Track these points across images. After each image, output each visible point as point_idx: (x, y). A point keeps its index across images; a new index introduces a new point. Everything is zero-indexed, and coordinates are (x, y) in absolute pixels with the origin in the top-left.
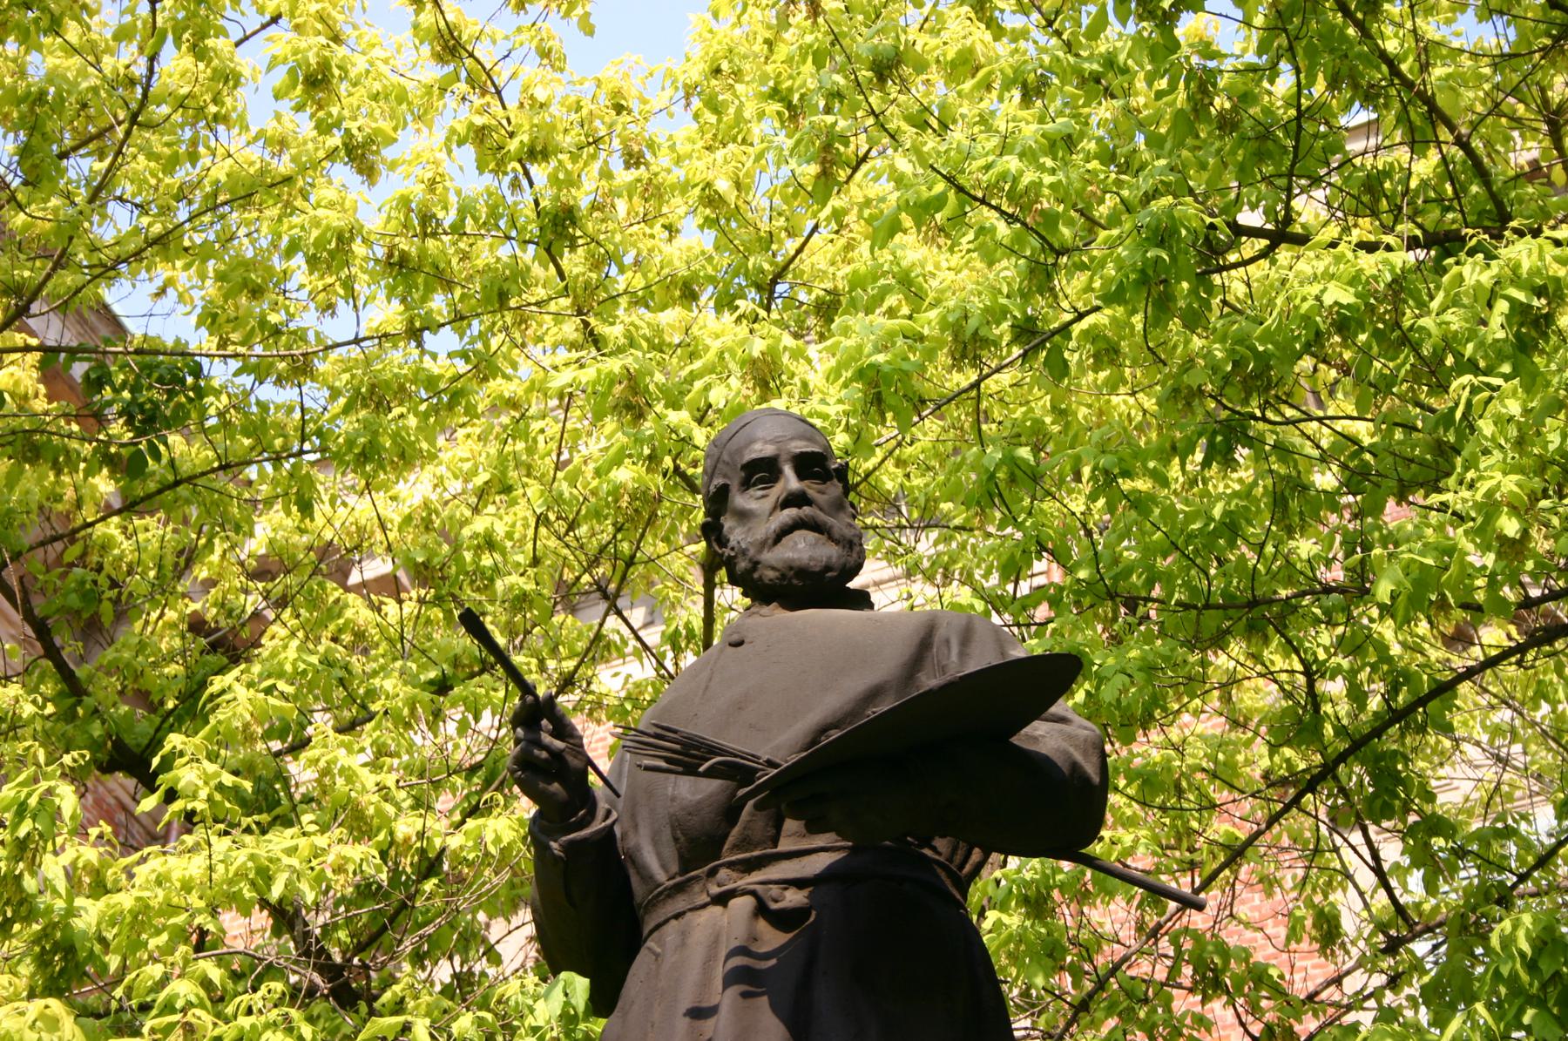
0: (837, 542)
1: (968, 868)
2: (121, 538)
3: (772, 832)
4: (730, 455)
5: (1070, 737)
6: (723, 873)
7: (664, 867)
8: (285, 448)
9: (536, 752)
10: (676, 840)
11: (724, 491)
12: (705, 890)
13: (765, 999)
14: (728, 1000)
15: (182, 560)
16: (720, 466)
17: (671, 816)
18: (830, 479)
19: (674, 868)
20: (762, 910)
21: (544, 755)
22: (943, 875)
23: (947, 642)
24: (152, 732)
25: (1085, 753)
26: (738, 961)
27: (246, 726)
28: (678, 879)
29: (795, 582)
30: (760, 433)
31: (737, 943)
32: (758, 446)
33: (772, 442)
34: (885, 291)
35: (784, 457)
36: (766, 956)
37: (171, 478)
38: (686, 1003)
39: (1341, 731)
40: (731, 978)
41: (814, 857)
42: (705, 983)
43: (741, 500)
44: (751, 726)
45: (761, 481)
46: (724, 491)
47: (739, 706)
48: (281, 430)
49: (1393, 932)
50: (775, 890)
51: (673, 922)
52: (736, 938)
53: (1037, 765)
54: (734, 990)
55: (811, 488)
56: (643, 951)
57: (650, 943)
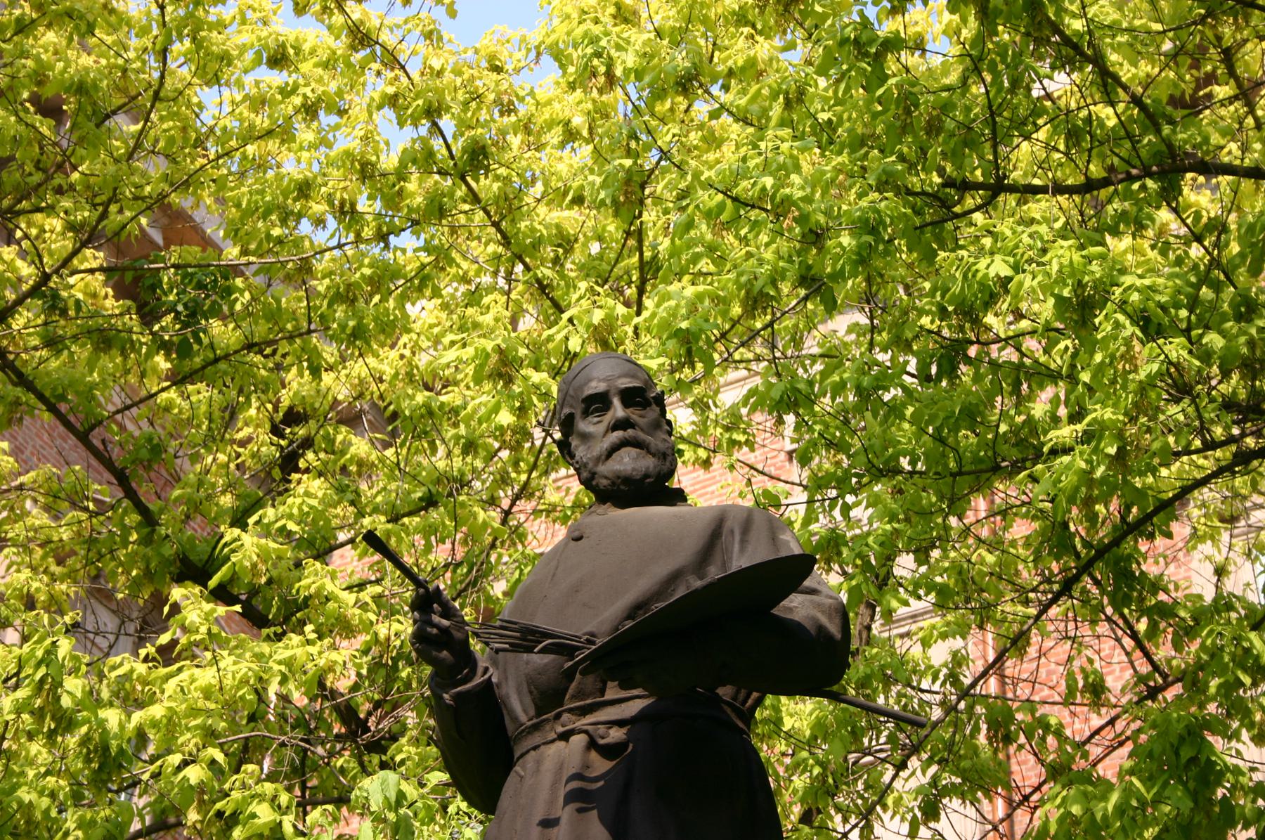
0: (654, 455)
1: (750, 702)
2: (179, 401)
3: (599, 685)
4: (575, 390)
5: (819, 606)
6: (565, 716)
7: (525, 711)
8: (296, 328)
9: (429, 629)
10: (531, 692)
11: (571, 417)
12: (553, 729)
13: (595, 812)
14: (567, 814)
15: (227, 415)
16: (568, 398)
17: (527, 675)
18: (650, 405)
19: (532, 712)
20: (592, 744)
21: (435, 631)
22: (729, 711)
23: (732, 532)
24: (209, 550)
25: (830, 617)
26: (575, 784)
27: (254, 565)
28: (535, 721)
29: (622, 487)
30: (595, 374)
31: (574, 771)
32: (594, 384)
33: (604, 380)
34: (695, 259)
35: (613, 391)
36: (596, 779)
37: (211, 356)
38: (538, 817)
39: (1087, 544)
40: (571, 797)
41: (631, 703)
42: (551, 802)
43: (584, 426)
44: (584, 605)
45: (597, 410)
46: (571, 417)
47: (576, 589)
48: (294, 316)
49: (1152, 684)
50: (602, 729)
51: (533, 753)
52: (572, 768)
53: (792, 629)
54: (571, 807)
55: (634, 414)
56: (512, 774)
57: (517, 768)
